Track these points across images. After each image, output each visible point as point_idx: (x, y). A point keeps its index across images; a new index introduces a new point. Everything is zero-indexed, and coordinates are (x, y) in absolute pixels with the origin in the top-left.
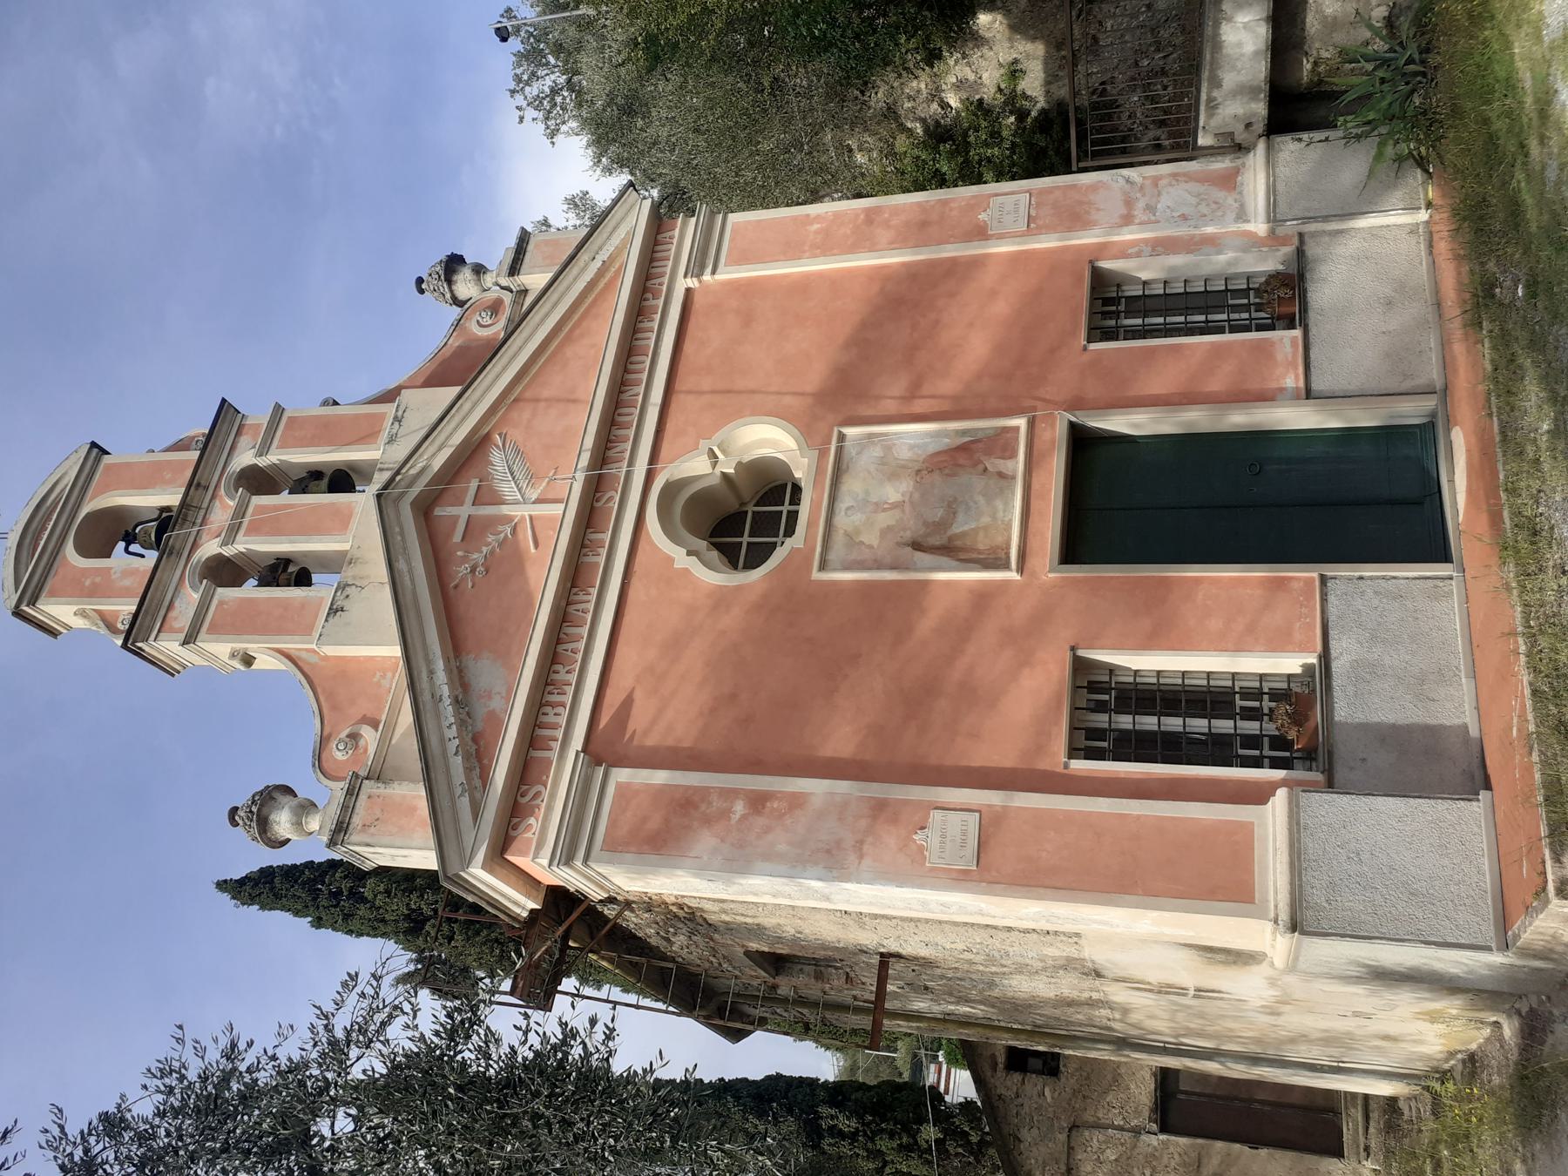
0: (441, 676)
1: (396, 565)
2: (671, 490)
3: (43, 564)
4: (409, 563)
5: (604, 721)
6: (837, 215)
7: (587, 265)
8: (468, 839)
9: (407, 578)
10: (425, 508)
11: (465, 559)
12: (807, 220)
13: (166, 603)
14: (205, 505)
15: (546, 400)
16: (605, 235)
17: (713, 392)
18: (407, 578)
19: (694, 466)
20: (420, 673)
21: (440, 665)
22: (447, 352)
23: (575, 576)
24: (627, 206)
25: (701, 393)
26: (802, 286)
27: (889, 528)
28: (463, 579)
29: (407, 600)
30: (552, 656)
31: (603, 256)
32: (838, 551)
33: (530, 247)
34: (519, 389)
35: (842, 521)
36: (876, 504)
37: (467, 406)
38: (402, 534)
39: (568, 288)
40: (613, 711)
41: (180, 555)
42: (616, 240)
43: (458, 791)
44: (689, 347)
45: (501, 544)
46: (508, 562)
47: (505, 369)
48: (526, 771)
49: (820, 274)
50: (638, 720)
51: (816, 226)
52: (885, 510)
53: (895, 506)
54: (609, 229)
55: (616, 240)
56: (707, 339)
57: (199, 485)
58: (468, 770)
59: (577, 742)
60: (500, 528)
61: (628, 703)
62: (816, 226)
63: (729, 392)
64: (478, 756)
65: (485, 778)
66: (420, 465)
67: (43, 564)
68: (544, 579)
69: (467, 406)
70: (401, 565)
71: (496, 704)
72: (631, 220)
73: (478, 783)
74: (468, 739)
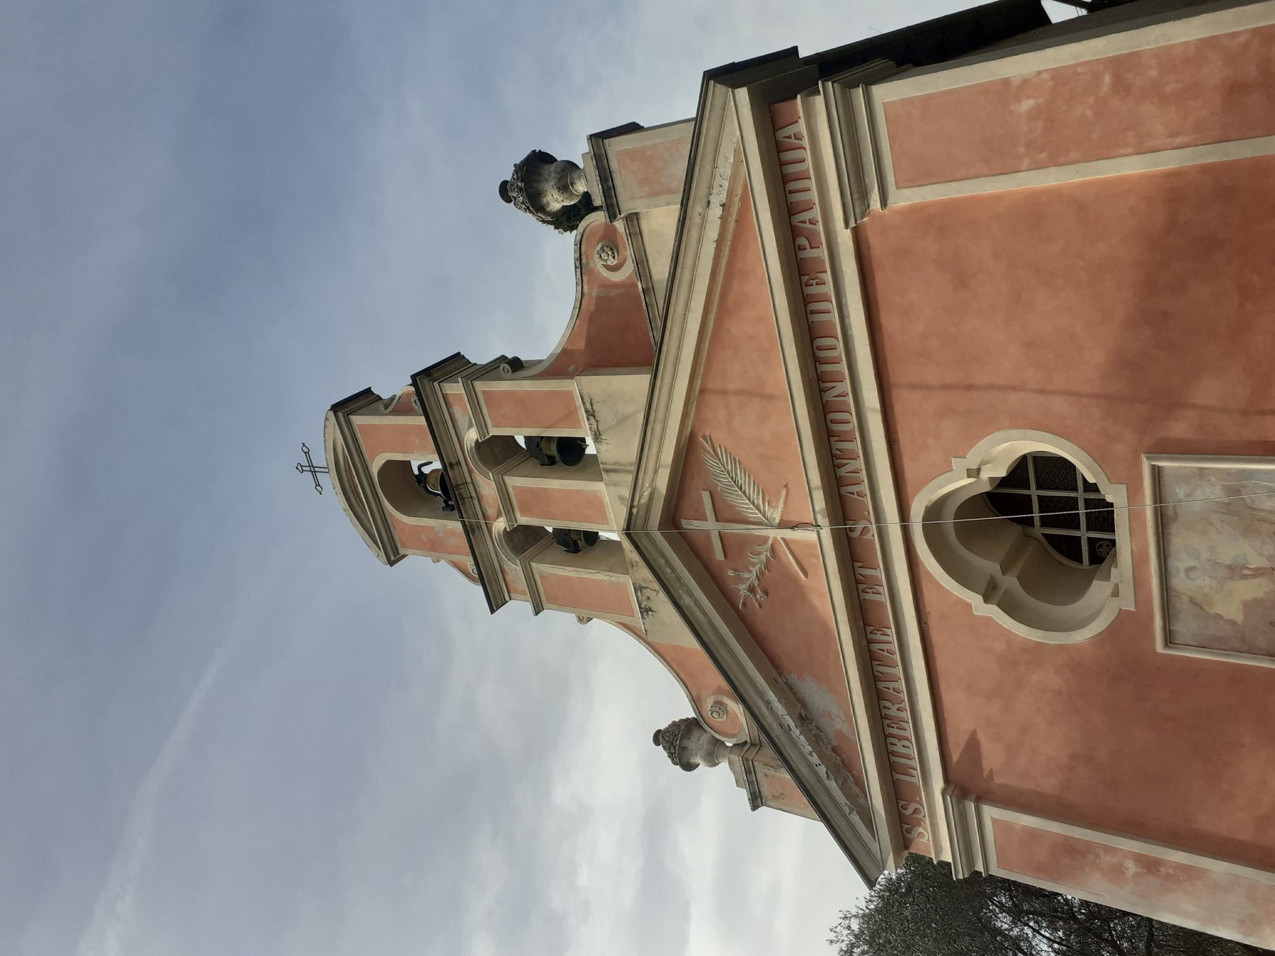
0: (779, 708)
1: (682, 603)
2: (934, 512)
3: (384, 534)
4: (691, 595)
5: (955, 756)
6: (1060, 77)
7: (704, 218)
8: (875, 847)
9: (698, 613)
10: (671, 519)
11: (740, 580)
12: (1005, 91)
13: (498, 570)
14: (469, 480)
15: (738, 393)
16: (708, 168)
17: (944, 387)
18: (698, 613)
19: (956, 482)
20: (759, 710)
21: (771, 696)
22: (589, 305)
23: (851, 553)
24: (718, 110)
25: (927, 387)
26: (1033, 212)
27: (1256, 602)
28: (746, 597)
29: (710, 636)
30: (870, 660)
31: (718, 198)
32: (1186, 626)
33: (614, 165)
34: (698, 383)
35: (1179, 582)
36: (1230, 567)
37: (658, 428)
38: (669, 564)
39: (697, 255)
40: (960, 751)
41: (480, 527)
42: (725, 167)
43: (847, 810)
44: (889, 322)
45: (768, 564)
46: (781, 584)
47: (674, 377)
48: (897, 793)
49: (1055, 195)
50: (992, 757)
51: (1027, 105)
52: (1244, 577)
53: (1258, 573)
54: (709, 157)
55: (725, 167)
56: (915, 303)
57: (451, 465)
58: (843, 787)
59: (938, 783)
60: (758, 549)
61: (973, 745)
62: (1027, 105)
63: (970, 387)
64: (843, 764)
65: (860, 783)
66: (646, 494)
67: (384, 534)
68: (827, 593)
69: (658, 428)
70: (686, 600)
71: (839, 725)
72: (732, 129)
73: (856, 789)
74: (829, 752)
